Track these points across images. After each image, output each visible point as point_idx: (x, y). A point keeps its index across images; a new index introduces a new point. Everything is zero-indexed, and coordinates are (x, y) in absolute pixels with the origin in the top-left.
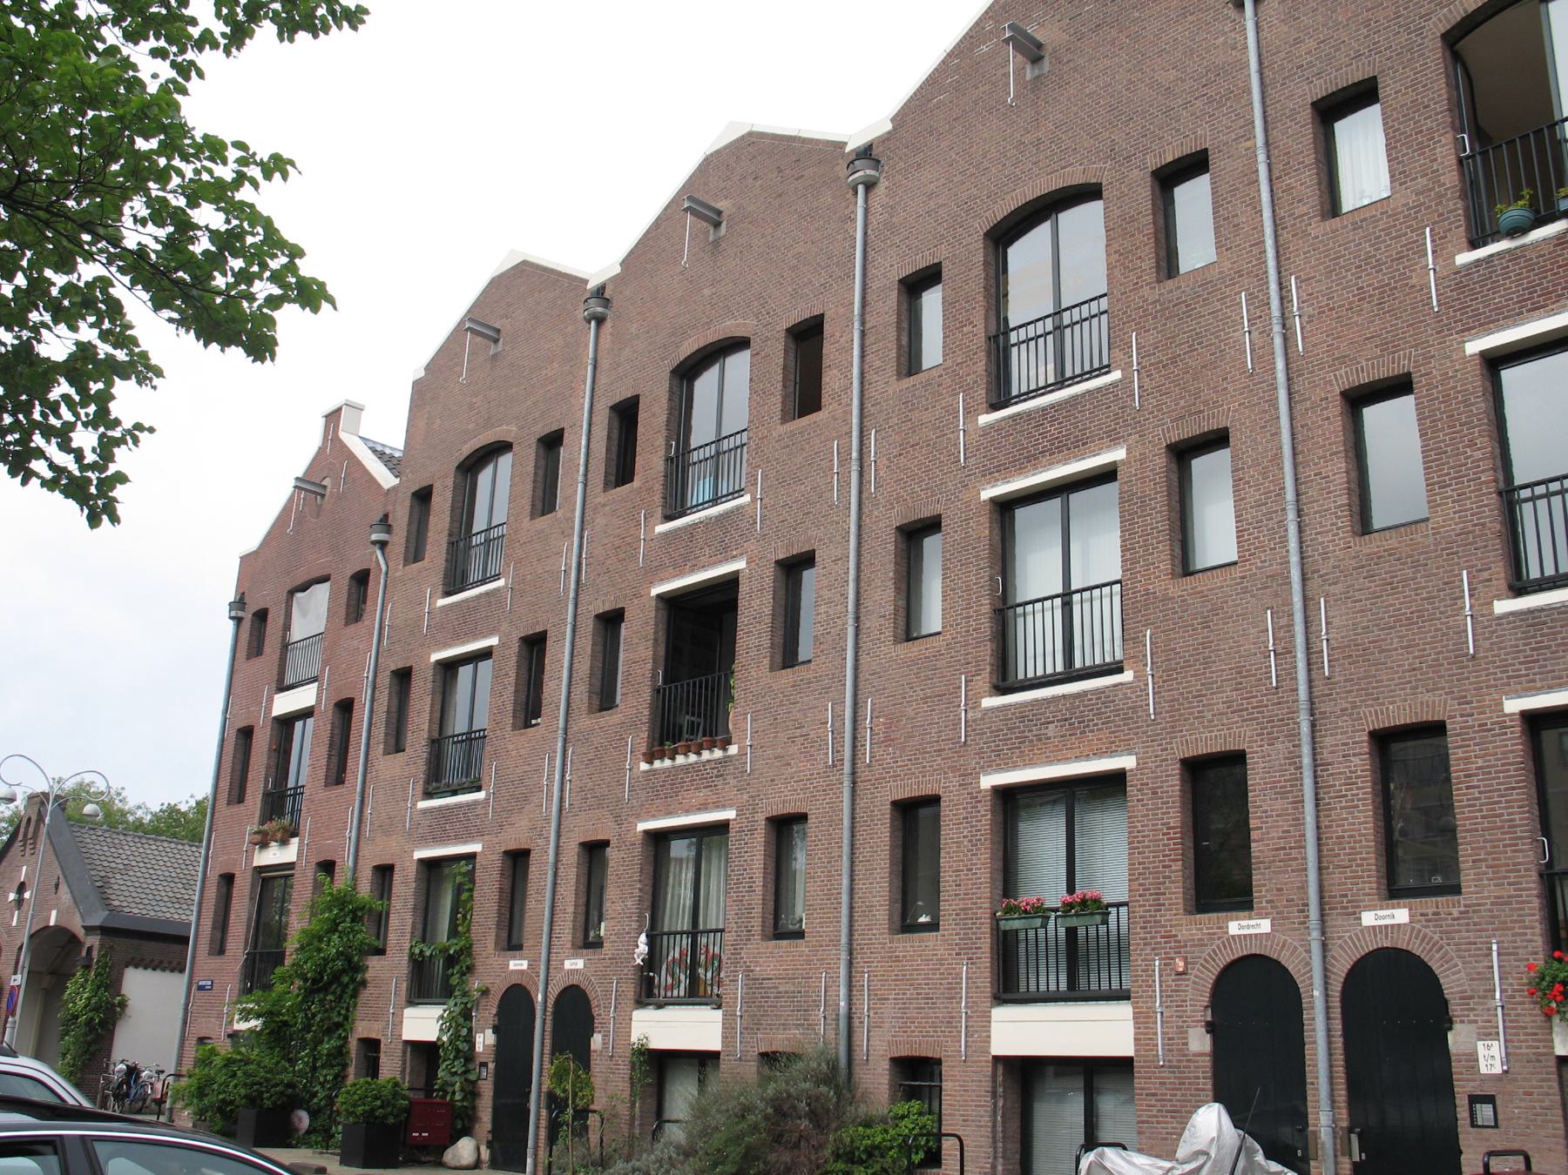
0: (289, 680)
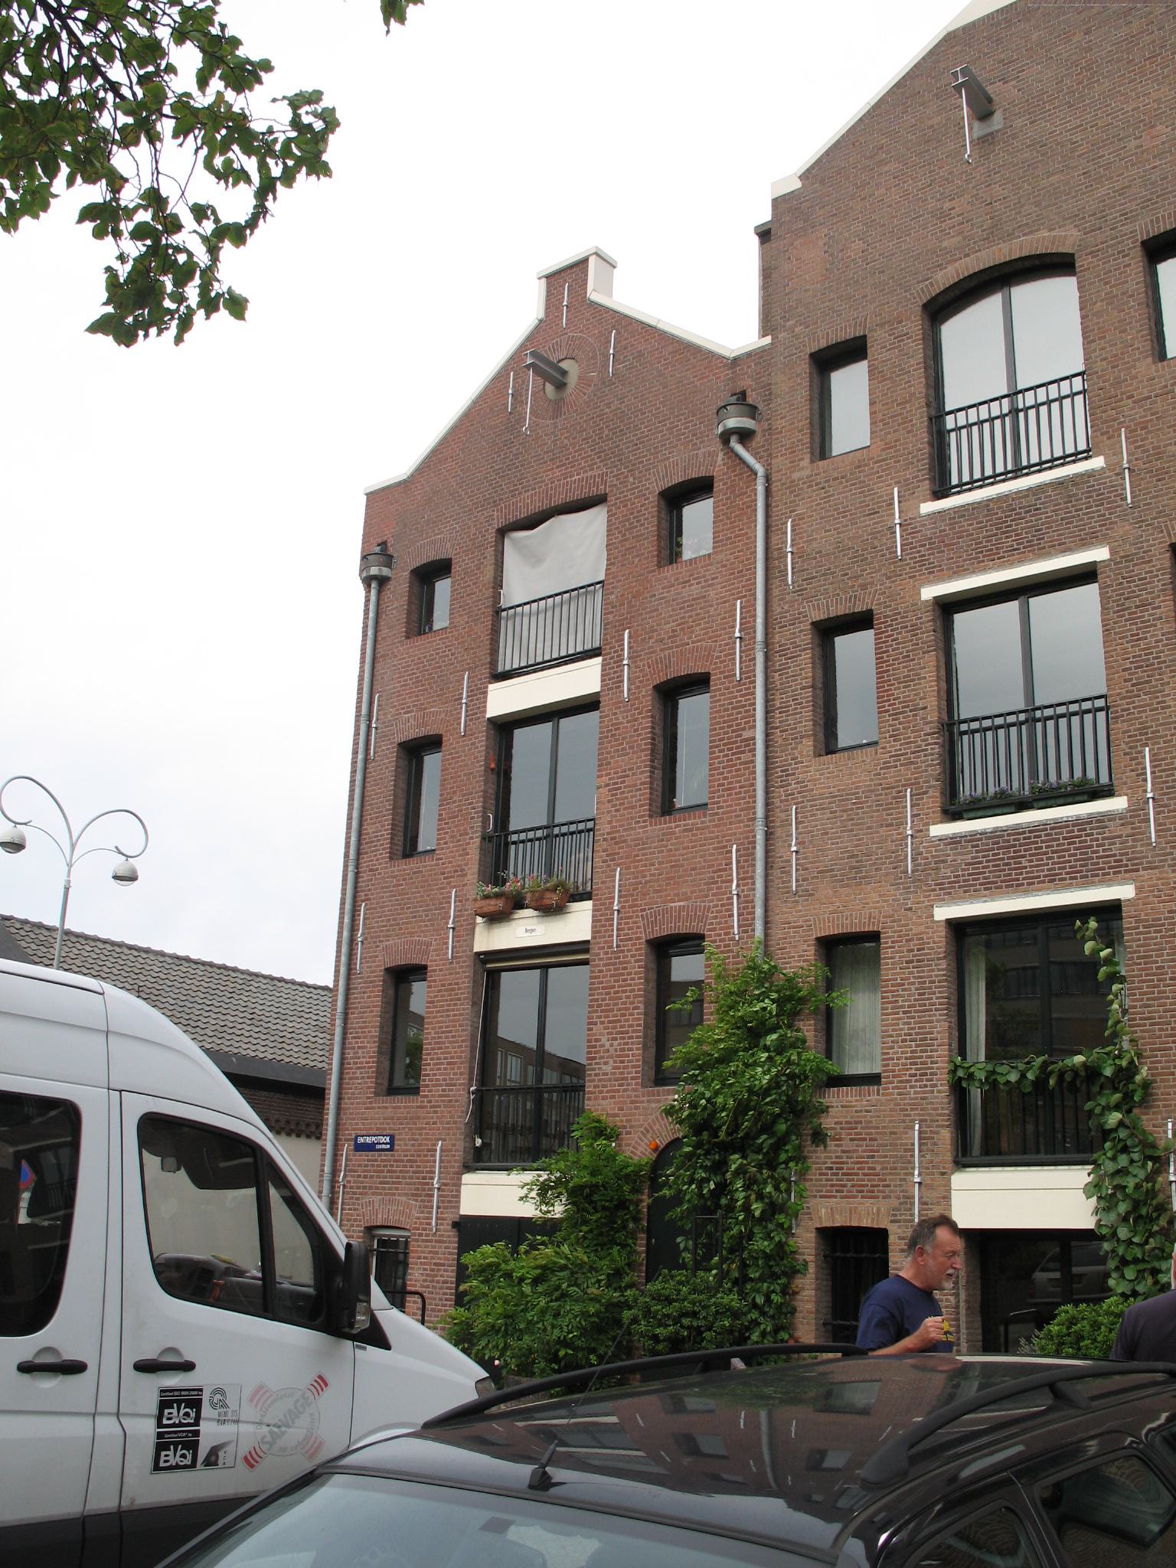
0: (505, 664)
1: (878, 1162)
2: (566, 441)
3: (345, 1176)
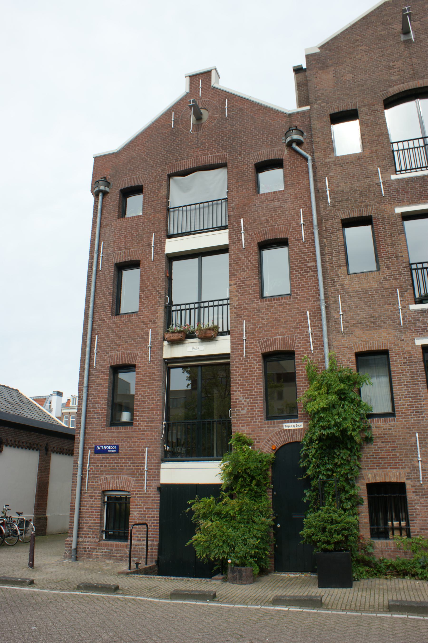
1: (397, 452)
2: (204, 141)
3: (89, 466)
